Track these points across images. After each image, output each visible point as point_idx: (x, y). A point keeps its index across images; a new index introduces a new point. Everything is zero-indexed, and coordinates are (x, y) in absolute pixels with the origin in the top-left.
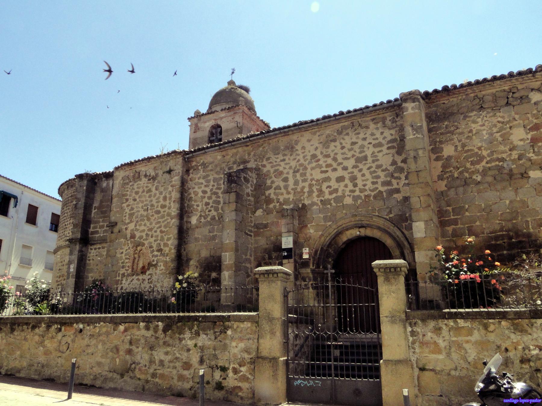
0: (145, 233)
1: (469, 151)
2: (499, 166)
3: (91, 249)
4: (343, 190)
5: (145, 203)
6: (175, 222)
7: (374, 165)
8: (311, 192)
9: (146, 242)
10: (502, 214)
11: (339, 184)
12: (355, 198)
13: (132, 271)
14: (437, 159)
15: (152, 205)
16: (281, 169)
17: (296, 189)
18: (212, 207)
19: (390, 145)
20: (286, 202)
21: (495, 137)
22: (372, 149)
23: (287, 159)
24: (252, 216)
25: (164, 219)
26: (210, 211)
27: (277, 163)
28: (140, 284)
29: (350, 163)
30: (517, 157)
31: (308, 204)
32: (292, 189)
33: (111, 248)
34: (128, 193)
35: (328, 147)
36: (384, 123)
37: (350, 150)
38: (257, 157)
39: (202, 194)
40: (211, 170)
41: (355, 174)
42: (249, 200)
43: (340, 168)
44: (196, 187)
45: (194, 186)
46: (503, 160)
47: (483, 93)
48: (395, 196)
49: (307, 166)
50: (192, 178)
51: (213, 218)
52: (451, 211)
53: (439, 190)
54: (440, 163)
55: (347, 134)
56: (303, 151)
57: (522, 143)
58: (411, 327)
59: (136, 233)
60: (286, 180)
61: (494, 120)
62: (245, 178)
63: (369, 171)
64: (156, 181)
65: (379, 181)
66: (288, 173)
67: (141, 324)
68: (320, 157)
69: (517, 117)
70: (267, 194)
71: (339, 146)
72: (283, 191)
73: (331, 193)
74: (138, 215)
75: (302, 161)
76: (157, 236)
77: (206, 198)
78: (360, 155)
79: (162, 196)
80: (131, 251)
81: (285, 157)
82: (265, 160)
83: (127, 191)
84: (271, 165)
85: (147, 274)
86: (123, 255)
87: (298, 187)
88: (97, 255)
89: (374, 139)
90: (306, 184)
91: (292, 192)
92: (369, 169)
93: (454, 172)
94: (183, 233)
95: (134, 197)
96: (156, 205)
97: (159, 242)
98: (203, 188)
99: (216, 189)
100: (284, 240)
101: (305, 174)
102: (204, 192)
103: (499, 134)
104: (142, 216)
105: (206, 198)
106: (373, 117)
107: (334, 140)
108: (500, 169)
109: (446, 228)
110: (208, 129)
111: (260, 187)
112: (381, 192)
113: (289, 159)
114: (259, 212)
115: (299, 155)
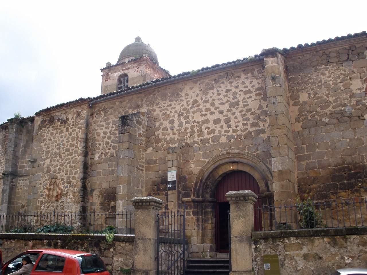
0: (58, 168)
1: (319, 98)
2: (342, 110)
3: (20, 180)
4: (219, 130)
5: (58, 142)
6: (80, 158)
7: (244, 109)
8: (192, 133)
9: (59, 175)
10: (344, 150)
11: (216, 125)
12: (229, 138)
13: (49, 199)
14: (295, 104)
15: (64, 144)
16: (168, 113)
17: (180, 130)
18: (111, 145)
19: (257, 92)
20: (172, 141)
21: (339, 86)
22: (243, 96)
23: (173, 104)
24: (144, 153)
25: (72, 156)
26: (109, 149)
27: (165, 108)
28: (55, 210)
29: (225, 108)
30: (355, 102)
31: (190, 143)
32: (177, 130)
33: (32, 180)
34: (45, 134)
35: (207, 94)
36: (252, 74)
37: (225, 96)
38: (149, 103)
39: (103, 135)
40: (111, 114)
41: (229, 116)
42: (141, 140)
43: (216, 112)
44: (99, 128)
45: (96, 127)
46: (345, 105)
47: (330, 50)
48: (261, 135)
49: (190, 110)
50: (95, 121)
51: (112, 156)
52: (305, 147)
53: (296, 130)
54: (297, 108)
55: (223, 83)
56: (187, 97)
57: (359, 92)
58: (255, 245)
59: (51, 167)
60: (172, 122)
61: (338, 73)
62: (137, 121)
63: (241, 114)
64: (67, 124)
65: (249, 122)
66: (174, 116)
67: (45, 241)
68: (200, 102)
69: (355, 70)
70: (156, 135)
71: (216, 93)
72: (169, 131)
73: (209, 133)
74: (52, 153)
75: (186, 106)
76: (67, 171)
77: (106, 138)
78: (233, 101)
79: (71, 137)
80: (48, 182)
81: (171, 103)
82: (155, 106)
83: (45, 132)
84: (160, 109)
85: (60, 201)
86: (42, 186)
87: (182, 128)
88: (24, 186)
89: (244, 87)
90: (189, 126)
91: (177, 132)
92: (240, 112)
93: (308, 116)
94: (87, 168)
95: (50, 137)
96: (66, 144)
97: (68, 175)
98: (104, 130)
99: (114, 130)
100: (169, 174)
101: (187, 117)
102: (105, 133)
103: (342, 84)
104: (55, 153)
105: (106, 138)
106: (244, 69)
107: (212, 88)
108: (342, 113)
109: (302, 162)
110: (117, 78)
111: (150, 130)
112: (250, 133)
113: (175, 104)
114: (150, 150)
115: (183, 101)
